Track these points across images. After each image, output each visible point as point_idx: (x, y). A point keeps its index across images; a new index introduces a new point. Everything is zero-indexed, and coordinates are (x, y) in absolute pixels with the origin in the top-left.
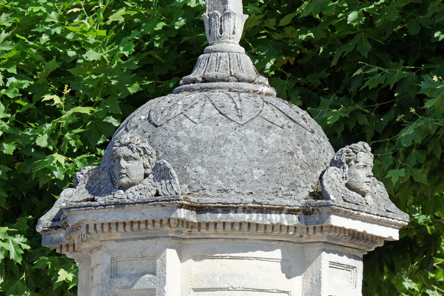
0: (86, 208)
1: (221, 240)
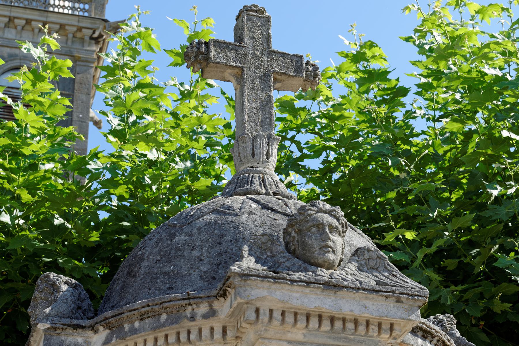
0: (276, 281)
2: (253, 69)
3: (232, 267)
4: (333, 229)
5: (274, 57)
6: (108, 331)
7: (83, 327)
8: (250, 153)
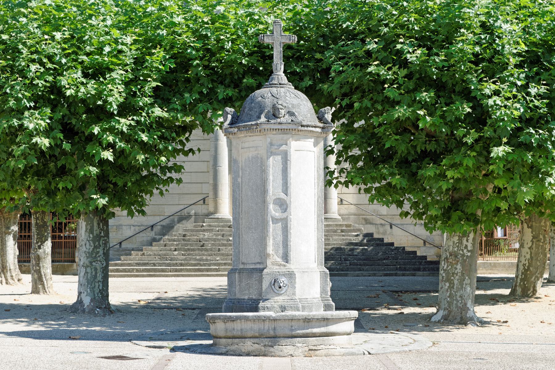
4: (281, 109)
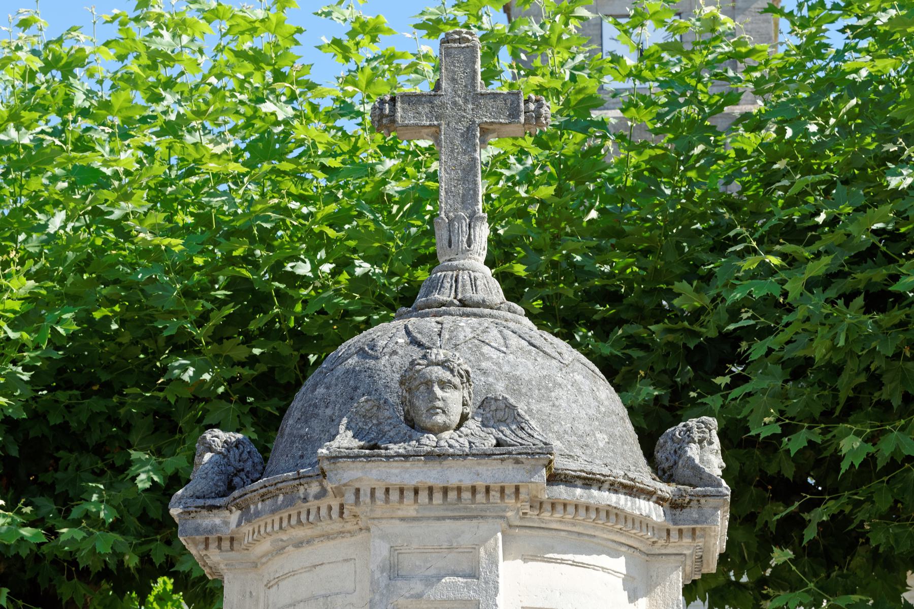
1: (563, 534)
2: (453, 124)
3: (320, 451)
4: (443, 385)
5: (482, 101)
6: (239, 512)
7: (218, 507)
8: (446, 243)
